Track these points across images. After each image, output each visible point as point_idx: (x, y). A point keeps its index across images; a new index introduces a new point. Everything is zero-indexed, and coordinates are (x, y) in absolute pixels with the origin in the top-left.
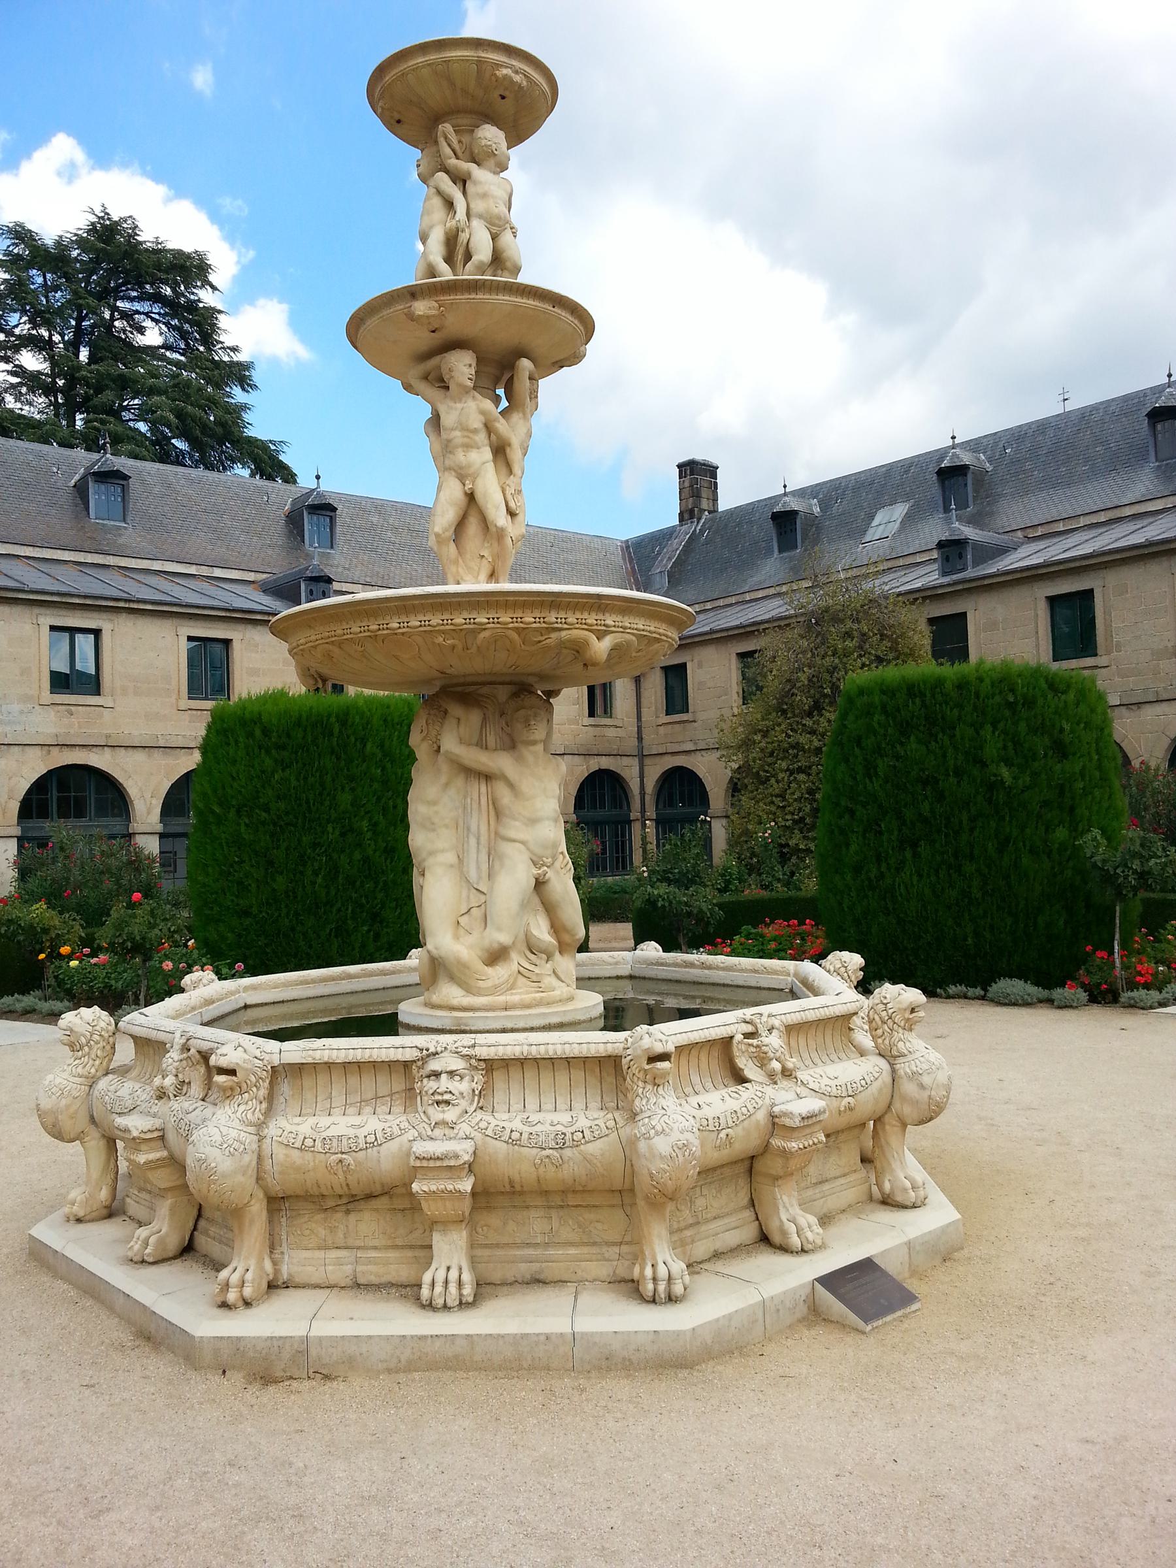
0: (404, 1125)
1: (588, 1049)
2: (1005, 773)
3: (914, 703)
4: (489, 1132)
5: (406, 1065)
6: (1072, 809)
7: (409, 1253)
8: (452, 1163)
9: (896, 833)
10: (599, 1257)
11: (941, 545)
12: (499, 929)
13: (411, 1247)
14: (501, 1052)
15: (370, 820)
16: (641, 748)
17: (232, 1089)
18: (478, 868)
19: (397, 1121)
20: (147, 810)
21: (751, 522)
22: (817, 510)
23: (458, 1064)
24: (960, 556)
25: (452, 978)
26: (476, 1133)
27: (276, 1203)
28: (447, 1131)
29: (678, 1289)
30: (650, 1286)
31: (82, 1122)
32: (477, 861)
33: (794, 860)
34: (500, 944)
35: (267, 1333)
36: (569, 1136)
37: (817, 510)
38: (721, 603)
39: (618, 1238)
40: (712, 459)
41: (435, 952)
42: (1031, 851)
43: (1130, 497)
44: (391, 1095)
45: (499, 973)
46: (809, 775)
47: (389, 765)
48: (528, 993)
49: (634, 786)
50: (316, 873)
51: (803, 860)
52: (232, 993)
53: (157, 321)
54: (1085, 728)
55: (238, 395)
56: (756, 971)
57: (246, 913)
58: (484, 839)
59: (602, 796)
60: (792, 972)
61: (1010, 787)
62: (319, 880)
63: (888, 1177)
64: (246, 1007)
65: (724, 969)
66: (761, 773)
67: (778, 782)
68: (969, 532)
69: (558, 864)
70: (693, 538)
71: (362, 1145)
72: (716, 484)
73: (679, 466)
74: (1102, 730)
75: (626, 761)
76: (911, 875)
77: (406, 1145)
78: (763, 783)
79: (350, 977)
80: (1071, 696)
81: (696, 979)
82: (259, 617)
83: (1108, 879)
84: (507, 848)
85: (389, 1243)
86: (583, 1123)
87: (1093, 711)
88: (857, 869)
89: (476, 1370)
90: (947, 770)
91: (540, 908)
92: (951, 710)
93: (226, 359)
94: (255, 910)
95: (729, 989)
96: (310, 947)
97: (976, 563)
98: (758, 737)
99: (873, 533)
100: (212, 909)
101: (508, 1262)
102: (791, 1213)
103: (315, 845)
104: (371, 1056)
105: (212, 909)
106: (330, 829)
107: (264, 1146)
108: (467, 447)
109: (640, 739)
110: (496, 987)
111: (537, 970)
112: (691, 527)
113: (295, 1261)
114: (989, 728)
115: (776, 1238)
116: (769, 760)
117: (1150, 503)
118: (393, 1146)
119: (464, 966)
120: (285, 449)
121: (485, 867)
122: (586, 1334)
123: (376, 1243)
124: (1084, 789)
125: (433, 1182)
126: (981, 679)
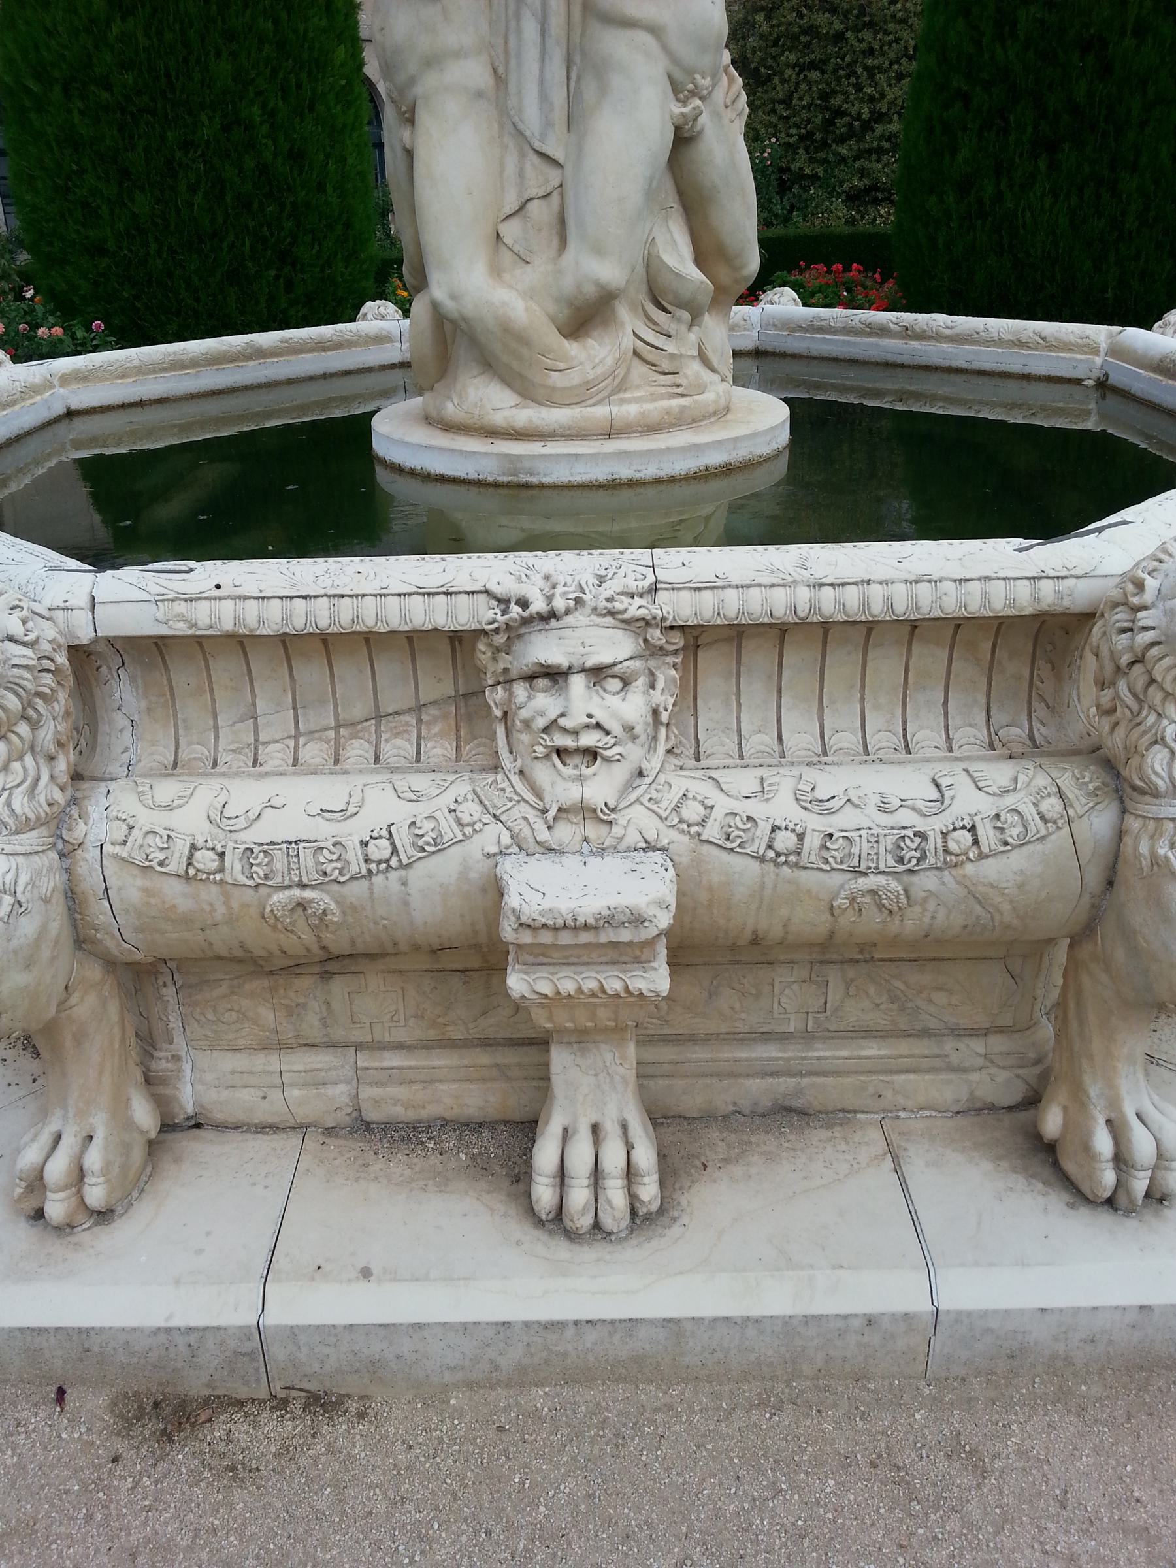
0: (470, 810)
1: (985, 595)
4: (712, 832)
5: (459, 643)
7: (484, 1058)
8: (625, 935)
9: (1029, 130)
10: (938, 1063)
12: (599, 251)
13: (486, 1043)
14: (732, 606)
15: (264, 106)
18: (544, 97)
19: (448, 799)
23: (614, 647)
25: (489, 365)
26: (674, 835)
28: (593, 831)
30: (1109, 1177)
32: (542, 81)
33: (796, 189)
34: (598, 283)
35: (156, 1320)
36: (935, 841)
39: (982, 1021)
41: (449, 306)
44: (418, 709)
45: (594, 355)
46: (823, 72)
47: (284, 15)
48: (654, 398)
50: (193, 189)
51: (806, 189)
52: (35, 390)
56: (1021, 344)
57: (99, 250)
58: (556, 22)
60: (1104, 346)
62: (198, 199)
64: (70, 414)
65: (951, 339)
66: (762, 70)
67: (783, 81)
69: (719, 95)
71: (356, 865)
77: (481, 865)
78: (763, 84)
79: (260, 353)
81: (890, 358)
84: (618, 46)
85: (432, 1034)
86: (968, 802)
89: (686, 1381)
91: (673, 202)
94: (111, 245)
95: (959, 379)
96: (197, 300)
98: (760, 17)
100: (51, 244)
101: (720, 1075)
103: (186, 145)
104: (356, 618)
105: (51, 244)
106: (204, 118)
107: (82, 869)
110: (588, 385)
111: (671, 347)
113: (209, 1077)
116: (773, 51)
118: (443, 869)
119: (516, 337)
121: (559, 97)
122: (969, 1314)
123: (400, 1035)
125: (566, 972)
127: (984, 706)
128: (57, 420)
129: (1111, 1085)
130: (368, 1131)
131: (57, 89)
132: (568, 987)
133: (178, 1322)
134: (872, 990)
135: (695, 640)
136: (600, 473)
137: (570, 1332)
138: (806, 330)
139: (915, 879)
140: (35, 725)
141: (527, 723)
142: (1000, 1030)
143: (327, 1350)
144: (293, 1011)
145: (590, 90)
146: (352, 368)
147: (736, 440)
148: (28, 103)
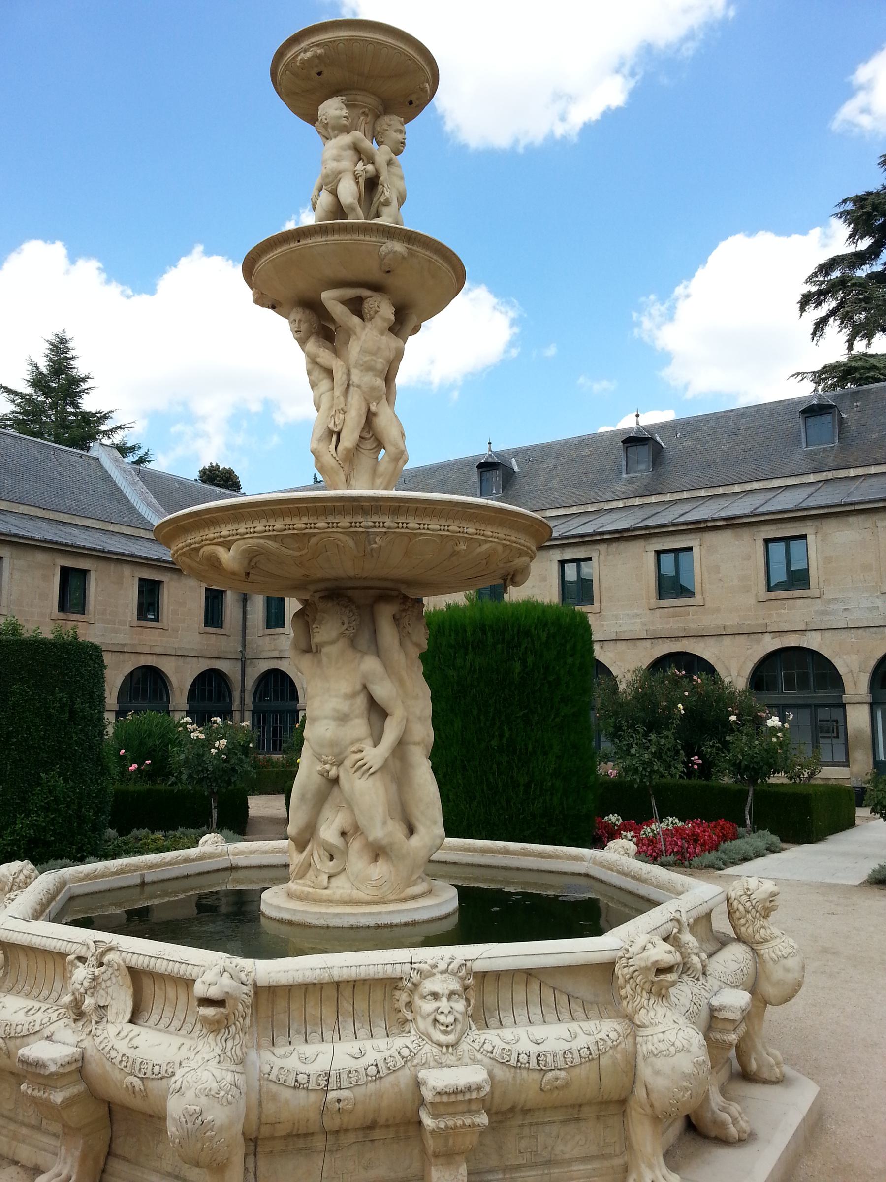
59: (210, 692)
63: (753, 1056)
64: (587, 875)
127: (793, 601)
135: (482, 976)
136: (371, 922)
146: (554, 870)
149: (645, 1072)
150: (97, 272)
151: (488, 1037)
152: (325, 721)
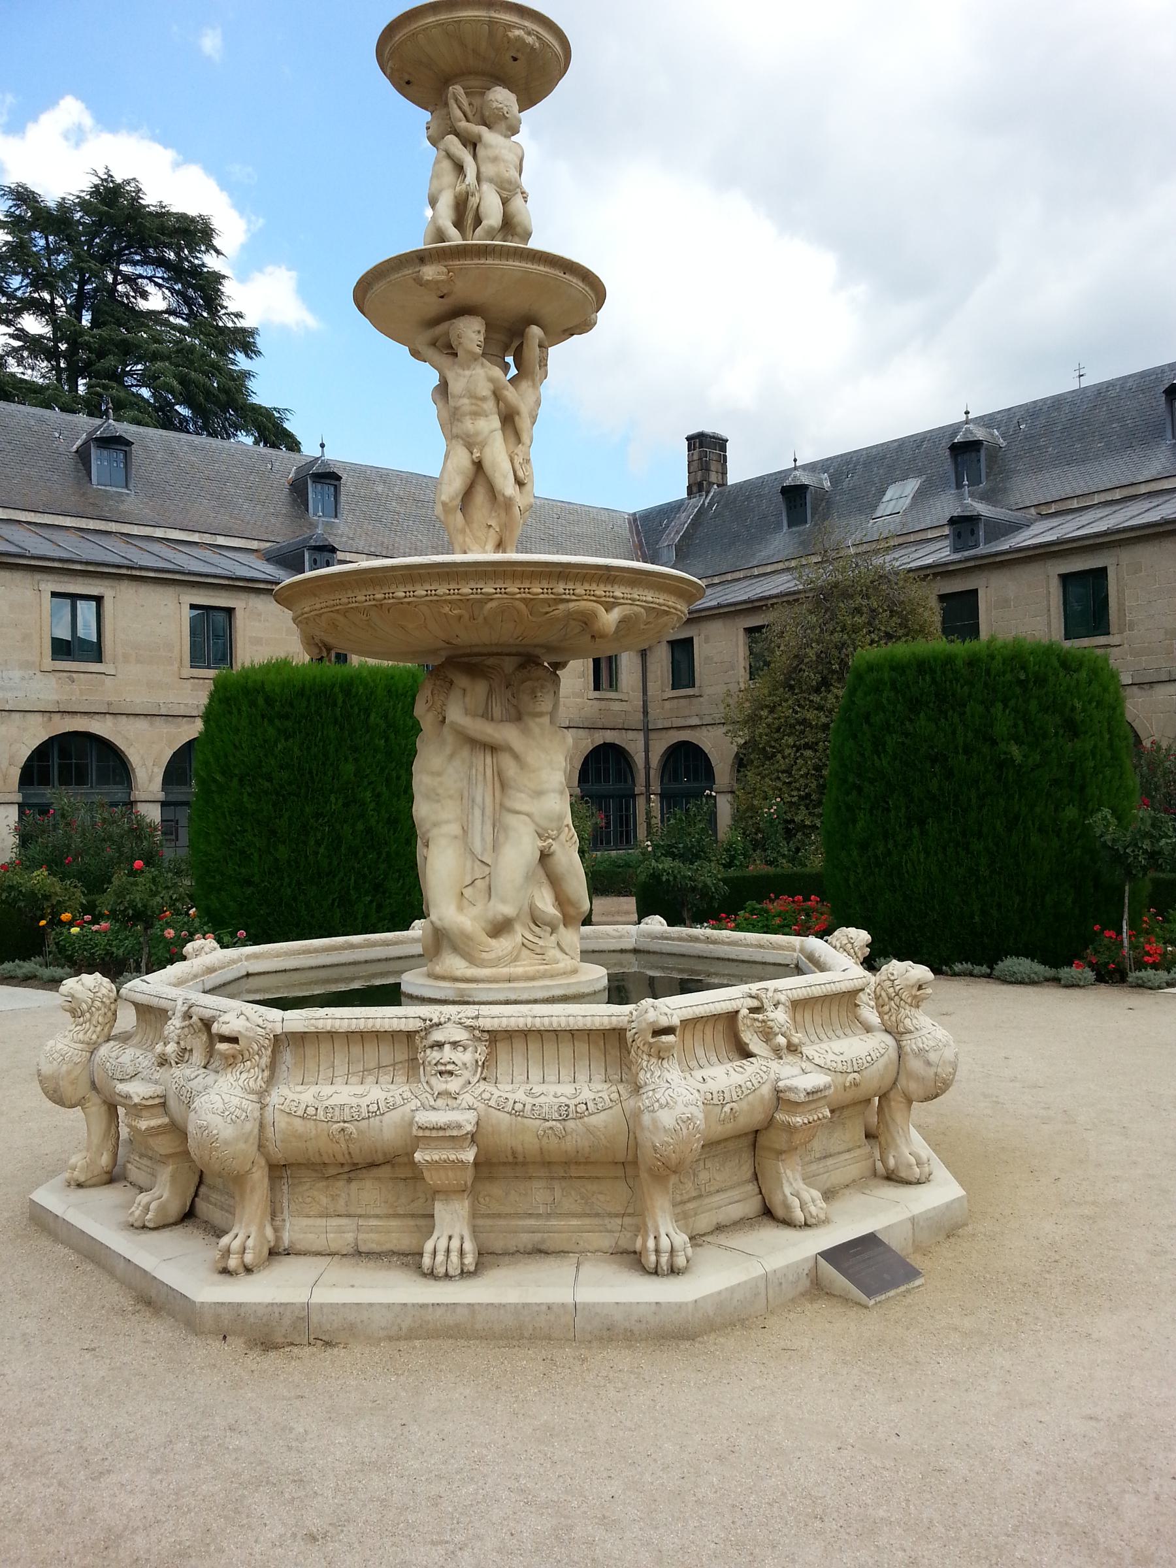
0: (407, 1094)
2: (1015, 751)
3: (924, 679)
5: (410, 1035)
6: (1082, 788)
8: (455, 1133)
9: (903, 810)
11: (953, 521)
12: (504, 901)
13: (413, 1216)
14: (504, 1024)
15: (374, 790)
16: (646, 723)
17: (234, 1057)
18: (483, 839)
19: (400, 1091)
20: (148, 778)
21: (759, 496)
22: (827, 484)
23: (461, 1035)
24: (973, 532)
25: (456, 949)
27: (278, 1171)
28: (450, 1101)
29: (681, 1261)
31: (83, 1089)
32: (482, 833)
33: (799, 836)
36: (572, 1107)
37: (827, 484)
38: (729, 577)
40: (722, 432)
41: (438, 923)
42: (1040, 830)
43: (1146, 475)
44: (394, 1065)
45: (504, 945)
46: (816, 751)
47: (392, 736)
48: (532, 965)
49: (639, 760)
50: (318, 843)
51: (808, 836)
52: (234, 962)
53: (160, 286)
54: (1097, 707)
55: (242, 362)
57: (248, 882)
59: (607, 770)
60: (798, 947)
61: (1020, 765)
64: (248, 975)
67: (784, 758)
68: (982, 508)
70: (702, 511)
72: (725, 457)
73: (688, 439)
74: (1114, 709)
75: (631, 735)
76: (918, 852)
78: (769, 759)
79: (352, 946)
80: (1083, 674)
82: (262, 586)
83: (1118, 858)
84: (512, 820)
85: (391, 1211)
86: (586, 1095)
87: (1105, 690)
88: (864, 846)
90: (956, 748)
91: (544, 880)
92: (962, 687)
93: (230, 325)
94: (256, 879)
96: (313, 916)
97: (988, 541)
99: (884, 508)
100: (214, 877)
102: (795, 1187)
103: (317, 815)
104: (373, 1026)
105: (214, 877)
107: (266, 1114)
108: (476, 415)
109: (645, 713)
111: (541, 943)
112: (699, 501)
113: (296, 1228)
114: (1000, 706)
115: (780, 1212)
117: (1165, 481)
118: (394, 1117)
119: (467, 937)
120: (289, 416)
121: (489, 839)
122: (588, 1304)
123: (378, 1211)
124: (1095, 767)
126: (992, 657)
128: (242, 977)
129: (655, 1222)
130: (359, 1254)
131: (235, 780)
132: (436, 1157)
133: (277, 1301)
134: (573, 1193)
137: (431, 1309)
138: (657, 938)
139: (567, 1123)
140: (260, 1057)
141: (429, 1063)
142: (629, 1215)
143: (334, 1317)
144: (334, 1198)
145: (501, 838)
147: (568, 984)
148: (214, 788)
149: (646, 1138)
150: (260, 342)
151: (488, 1088)
152: (552, 795)
